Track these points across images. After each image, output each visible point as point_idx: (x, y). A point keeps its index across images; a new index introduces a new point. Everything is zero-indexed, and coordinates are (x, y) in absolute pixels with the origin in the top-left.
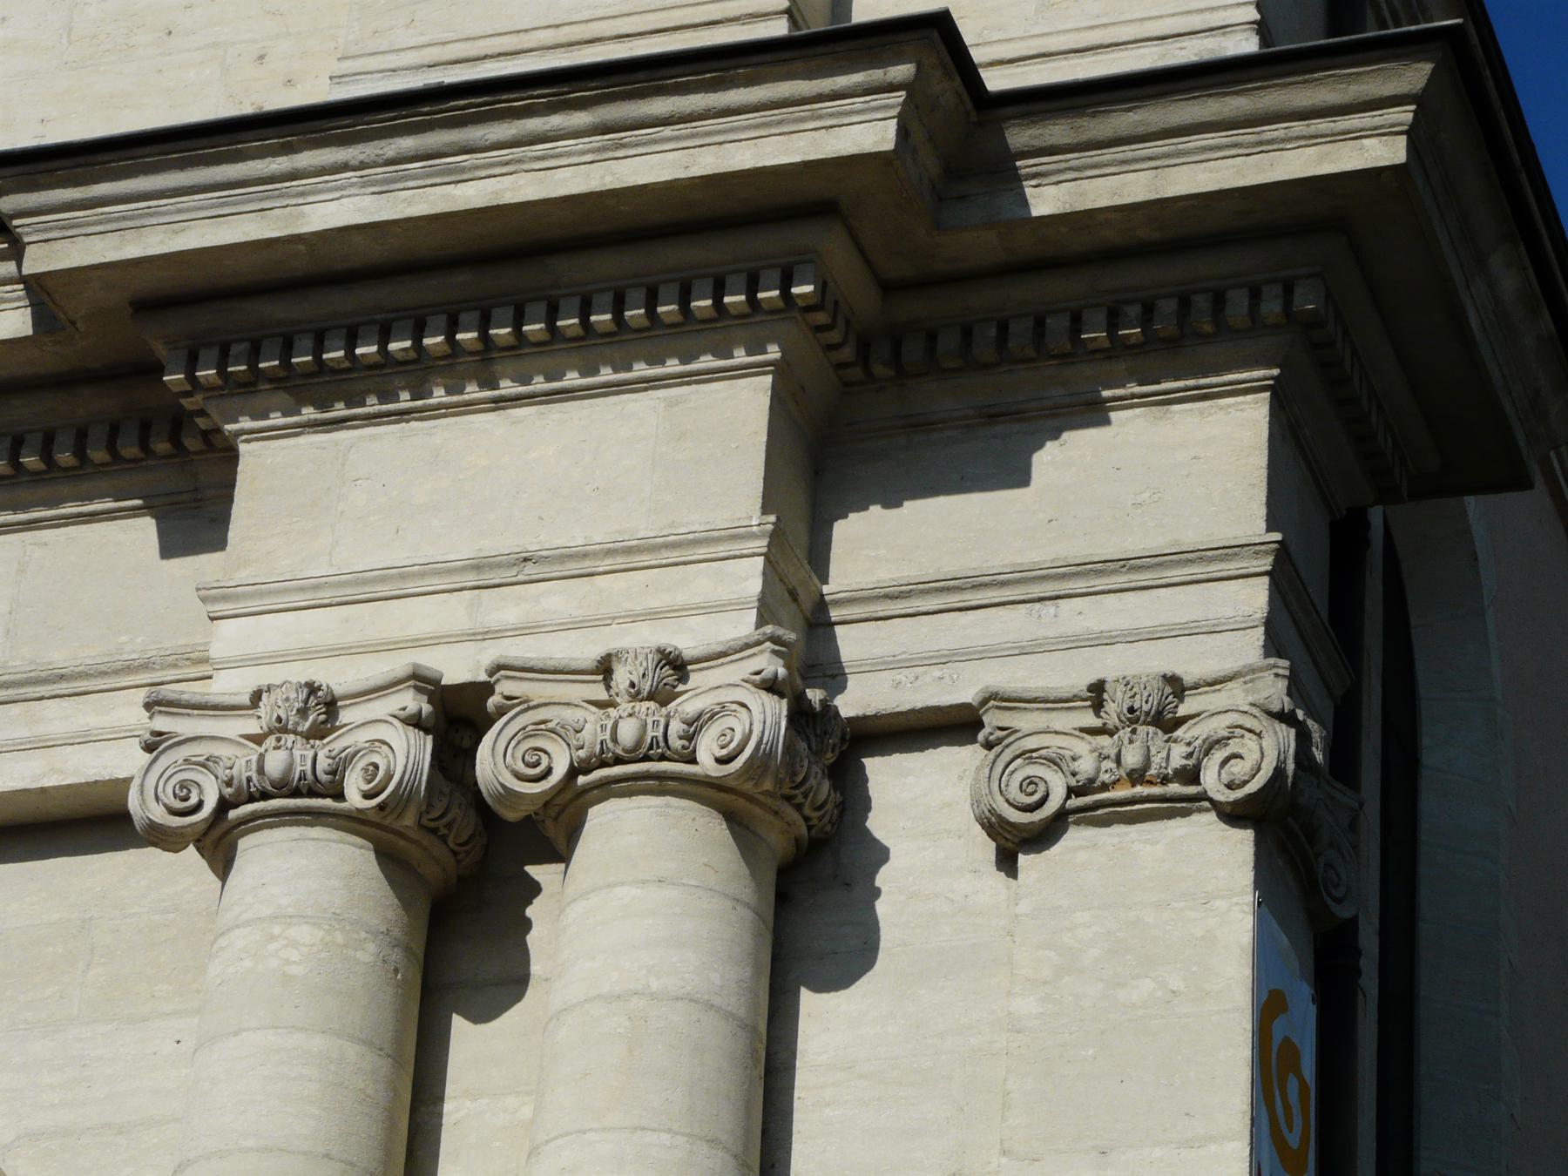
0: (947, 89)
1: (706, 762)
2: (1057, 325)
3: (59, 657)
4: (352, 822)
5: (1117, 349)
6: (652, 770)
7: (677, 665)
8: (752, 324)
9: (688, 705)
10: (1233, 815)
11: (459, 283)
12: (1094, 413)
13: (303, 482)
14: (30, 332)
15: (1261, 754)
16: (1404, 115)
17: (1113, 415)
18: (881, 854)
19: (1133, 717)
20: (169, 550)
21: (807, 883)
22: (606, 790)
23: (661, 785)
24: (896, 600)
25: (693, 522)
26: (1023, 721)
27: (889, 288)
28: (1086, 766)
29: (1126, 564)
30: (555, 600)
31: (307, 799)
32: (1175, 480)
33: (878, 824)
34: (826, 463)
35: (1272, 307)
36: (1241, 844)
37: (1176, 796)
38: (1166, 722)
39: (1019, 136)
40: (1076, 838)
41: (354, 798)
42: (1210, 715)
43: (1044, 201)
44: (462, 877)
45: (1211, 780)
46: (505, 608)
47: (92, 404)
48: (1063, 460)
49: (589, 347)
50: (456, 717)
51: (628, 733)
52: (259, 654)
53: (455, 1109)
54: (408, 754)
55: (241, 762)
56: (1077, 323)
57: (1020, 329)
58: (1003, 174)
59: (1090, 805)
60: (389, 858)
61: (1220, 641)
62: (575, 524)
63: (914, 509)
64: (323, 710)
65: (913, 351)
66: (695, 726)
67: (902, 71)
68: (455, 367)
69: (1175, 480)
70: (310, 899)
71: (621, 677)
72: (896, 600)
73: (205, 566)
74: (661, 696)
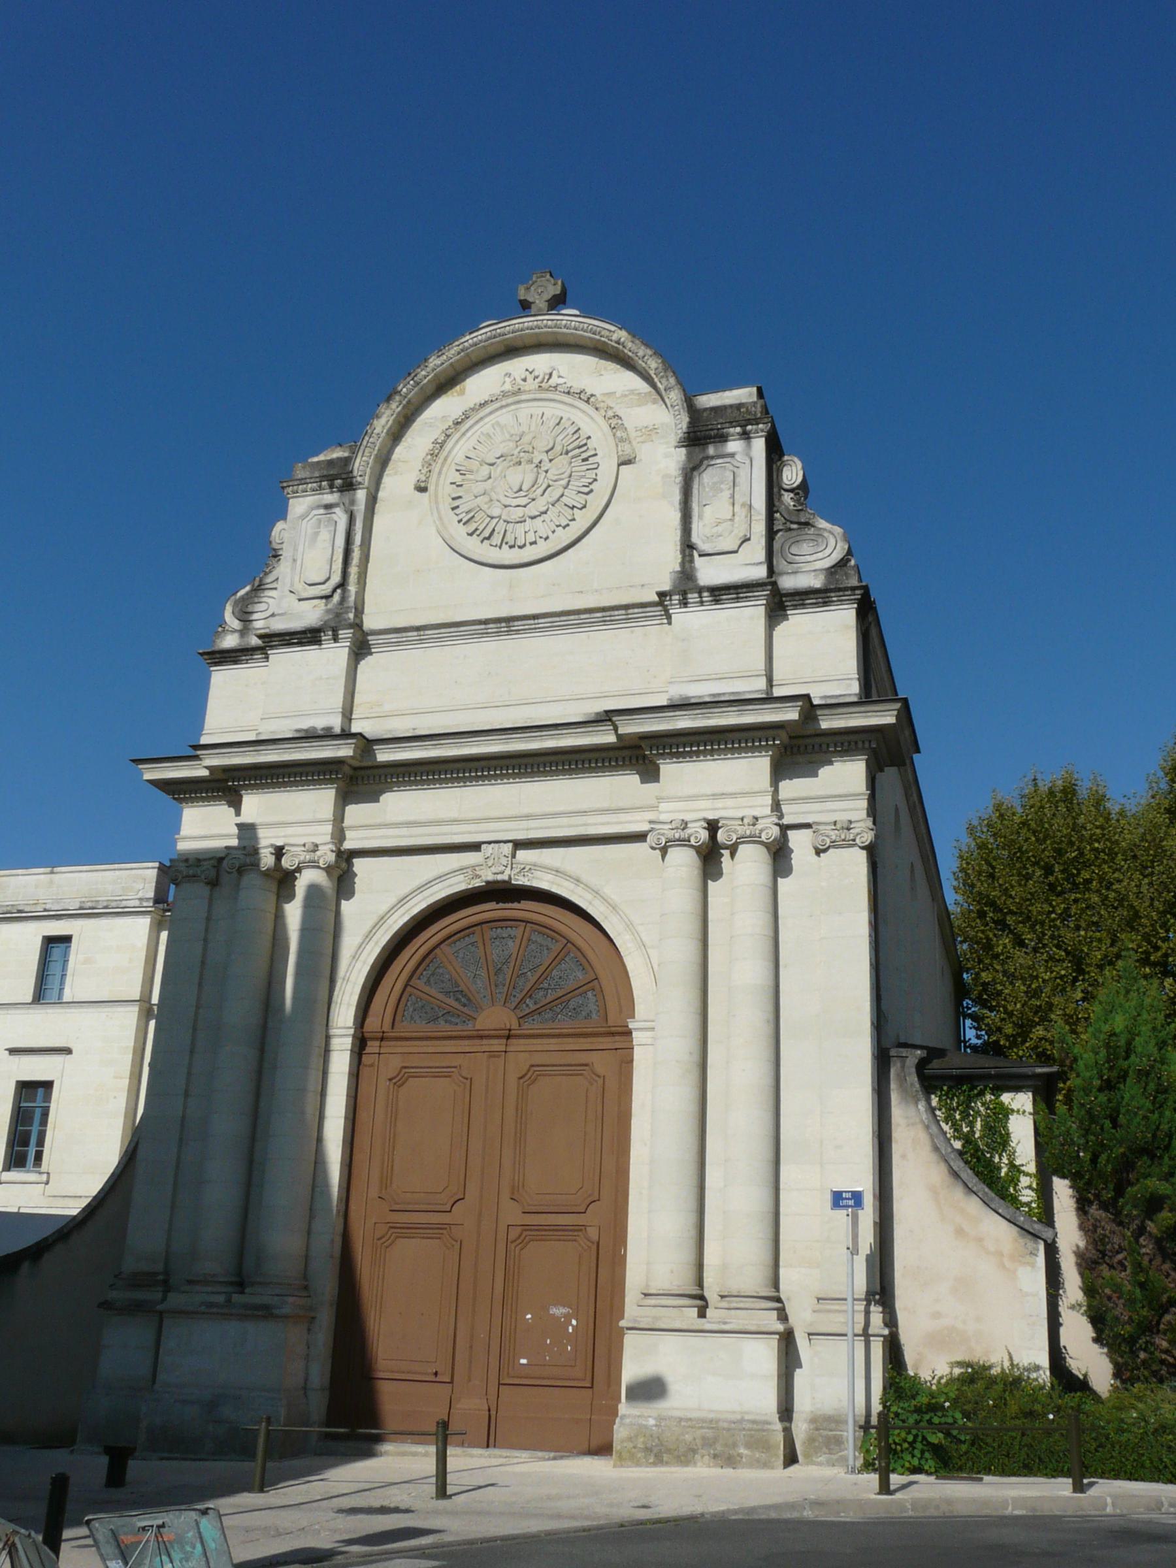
0: (808, 705)
1: (764, 838)
2: (824, 747)
3: (621, 804)
4: (692, 846)
5: (836, 751)
6: (754, 839)
7: (756, 819)
8: (767, 748)
9: (759, 827)
10: (863, 848)
11: (706, 737)
12: (831, 763)
13: (676, 774)
14: (1030, 1094)
15: (868, 838)
16: (895, 713)
17: (683, 450)
18: (792, 851)
19: (843, 828)
20: (642, 782)
21: (779, 856)
22: (743, 842)
23: (754, 842)
24: (794, 800)
25: (756, 789)
26: (821, 827)
27: (790, 737)
28: (834, 838)
29: (840, 796)
30: (729, 802)
31: (684, 842)
32: (847, 775)
33: (790, 845)
34: (779, 772)
35: (867, 745)
36: (864, 853)
37: (852, 844)
38: (849, 829)
39: (819, 712)
40: (831, 850)
41: (693, 842)
42: (858, 828)
43: (825, 725)
44: (711, 856)
45: (858, 841)
46: (719, 803)
47: (626, 753)
48: (824, 771)
49: (733, 750)
50: (713, 827)
51: (748, 833)
52: (670, 812)
53: (711, 899)
54: (704, 835)
55: (670, 834)
56: (828, 745)
57: (816, 747)
58: (815, 719)
59: (834, 845)
60: (698, 852)
61: (858, 810)
62: (731, 787)
63: (795, 780)
64: (685, 825)
65: (795, 750)
66: (761, 831)
67: (800, 703)
68: (705, 753)
69: (847, 775)
70: (684, 861)
71: (746, 821)
72: (794, 800)
73: (651, 787)
74: (754, 825)
